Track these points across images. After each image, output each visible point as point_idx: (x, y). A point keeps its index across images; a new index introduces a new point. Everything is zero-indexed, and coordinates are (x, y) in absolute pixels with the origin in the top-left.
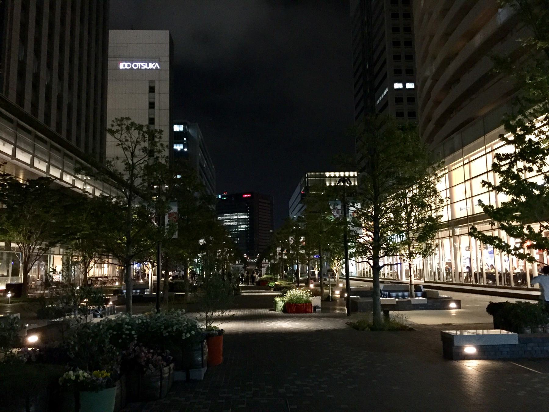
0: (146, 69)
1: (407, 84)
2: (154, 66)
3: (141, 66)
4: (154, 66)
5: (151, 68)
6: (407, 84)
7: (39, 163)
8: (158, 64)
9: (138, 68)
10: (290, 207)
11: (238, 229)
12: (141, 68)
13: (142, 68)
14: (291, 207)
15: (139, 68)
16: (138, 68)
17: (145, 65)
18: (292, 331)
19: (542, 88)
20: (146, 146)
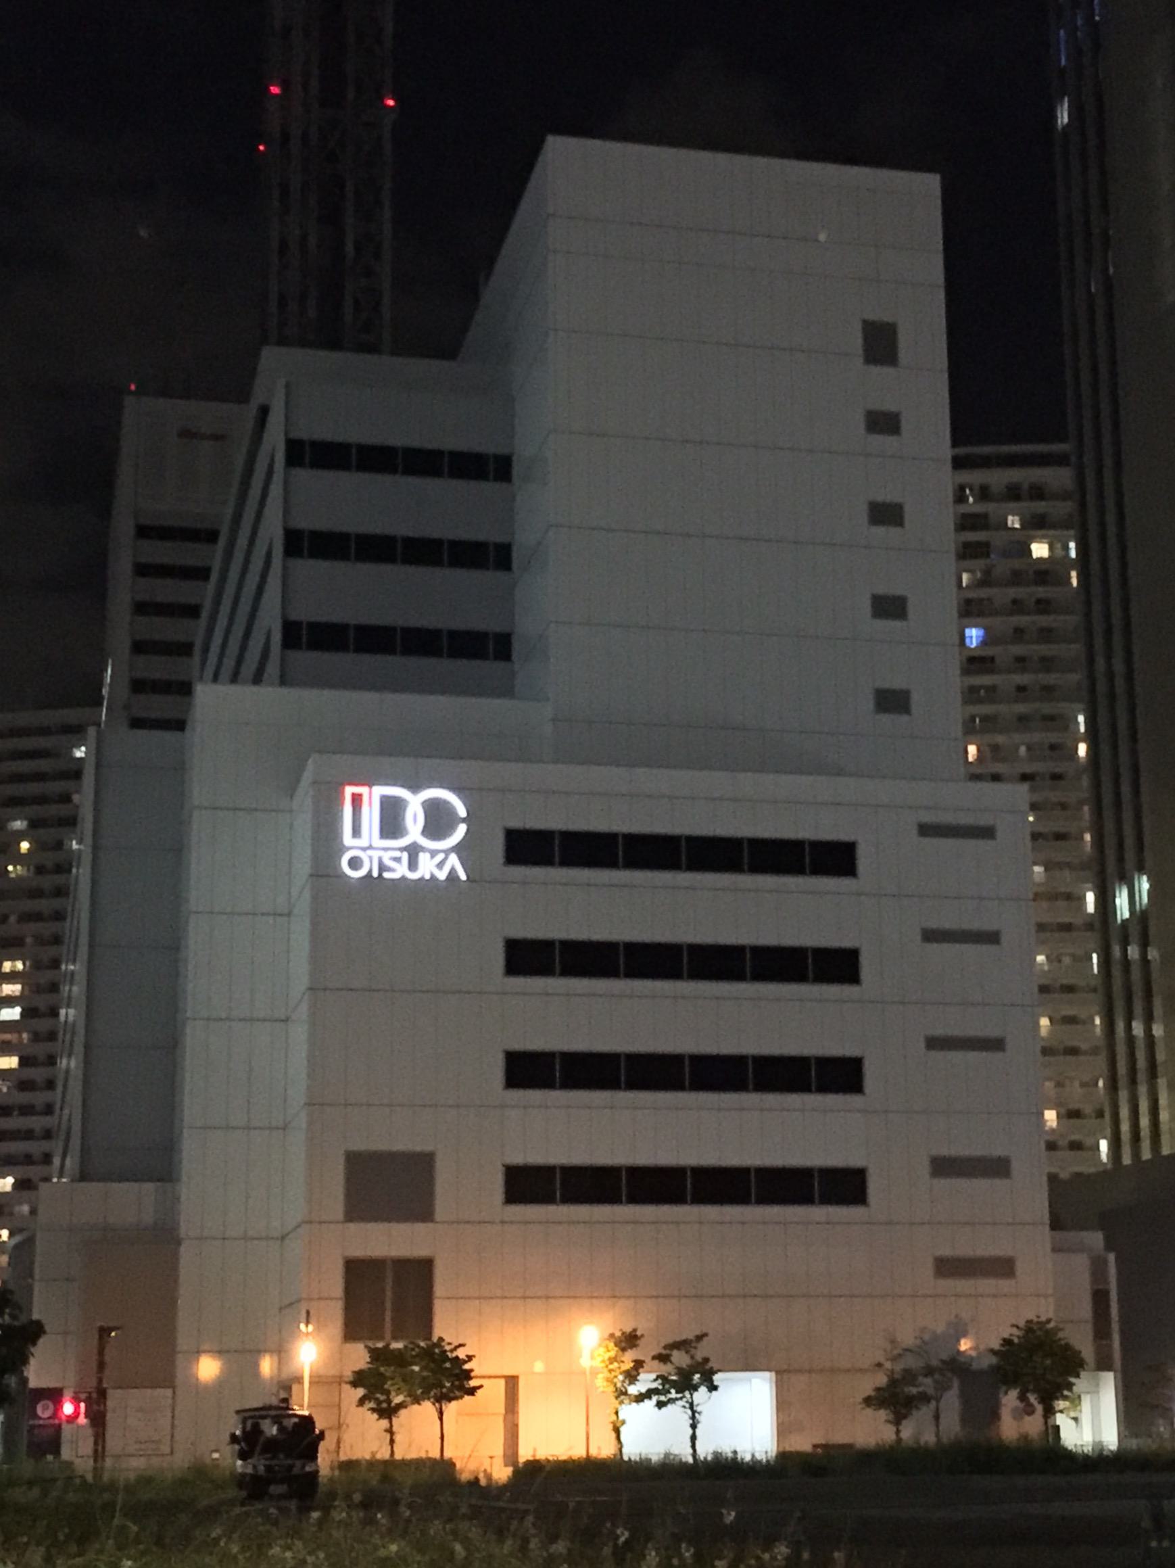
0: (403, 878)
1: (929, 185)
2: (440, 865)
3: (382, 867)
4: (440, 865)
5: (427, 877)
6: (929, 185)
7: (735, 1452)
8: (460, 858)
9: (370, 871)
10: (306, 997)
11: (1072, 564)
12: (380, 875)
13: (386, 875)
14: (303, 888)
15: (375, 874)
16: (370, 871)
17: (398, 860)
18: (801, 983)
19: (932, 1202)
20: (1006, 1336)
